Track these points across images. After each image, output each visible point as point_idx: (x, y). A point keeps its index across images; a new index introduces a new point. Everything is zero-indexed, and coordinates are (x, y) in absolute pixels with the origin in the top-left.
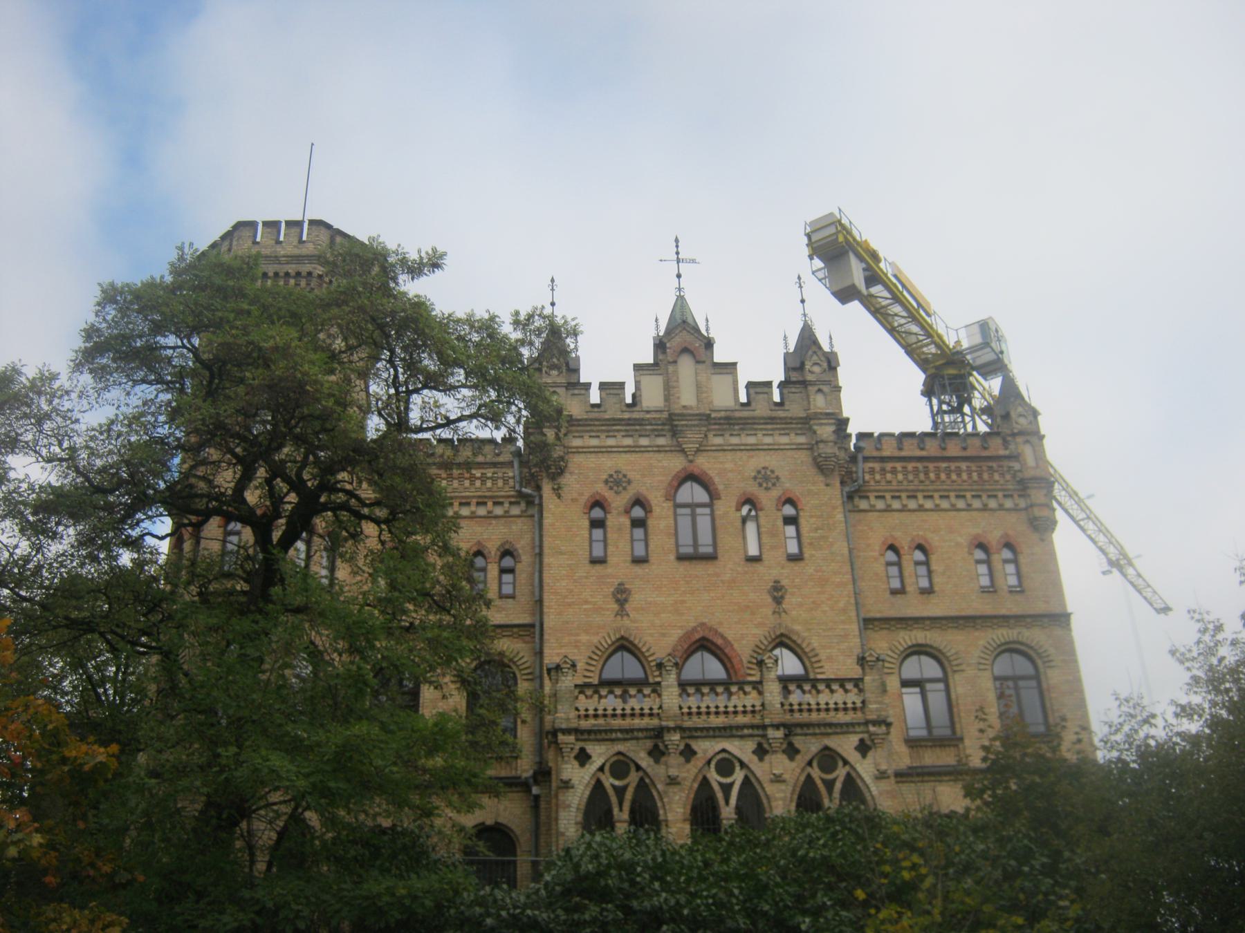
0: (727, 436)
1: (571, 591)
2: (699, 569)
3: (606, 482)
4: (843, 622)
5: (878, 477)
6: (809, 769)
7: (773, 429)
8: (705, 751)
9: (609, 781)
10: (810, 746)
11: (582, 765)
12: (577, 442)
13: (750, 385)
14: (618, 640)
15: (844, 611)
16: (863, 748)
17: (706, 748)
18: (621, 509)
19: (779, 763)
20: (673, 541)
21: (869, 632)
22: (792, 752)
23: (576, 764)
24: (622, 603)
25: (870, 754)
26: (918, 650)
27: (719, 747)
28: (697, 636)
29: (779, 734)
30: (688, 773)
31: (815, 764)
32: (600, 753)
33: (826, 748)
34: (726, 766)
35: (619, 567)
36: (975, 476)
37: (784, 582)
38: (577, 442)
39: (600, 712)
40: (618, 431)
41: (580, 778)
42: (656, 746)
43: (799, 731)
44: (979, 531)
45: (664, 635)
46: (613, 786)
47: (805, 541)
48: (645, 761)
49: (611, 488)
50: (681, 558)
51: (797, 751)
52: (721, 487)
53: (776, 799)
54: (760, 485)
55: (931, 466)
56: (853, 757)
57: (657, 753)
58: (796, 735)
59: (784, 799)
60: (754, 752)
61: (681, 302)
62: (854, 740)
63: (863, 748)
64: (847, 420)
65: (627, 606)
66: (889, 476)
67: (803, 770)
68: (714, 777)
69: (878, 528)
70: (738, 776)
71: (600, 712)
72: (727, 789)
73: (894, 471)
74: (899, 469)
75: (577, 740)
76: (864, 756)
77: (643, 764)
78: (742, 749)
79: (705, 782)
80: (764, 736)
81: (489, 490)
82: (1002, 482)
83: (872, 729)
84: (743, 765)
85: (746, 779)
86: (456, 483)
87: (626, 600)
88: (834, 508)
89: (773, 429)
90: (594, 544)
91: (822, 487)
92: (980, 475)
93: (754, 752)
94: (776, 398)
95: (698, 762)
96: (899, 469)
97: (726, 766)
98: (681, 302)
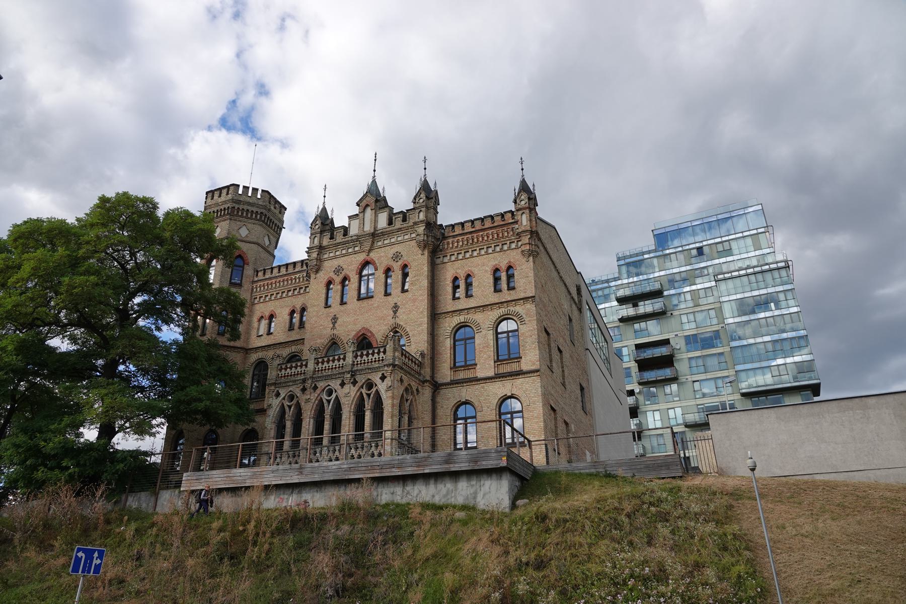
2: (365, 301)
9: (286, 403)
10: (361, 379)
15: (422, 312)
17: (321, 385)
22: (355, 383)
24: (334, 323)
25: (634, 348)
30: (314, 396)
35: (396, 296)
41: (275, 403)
55: (475, 235)
61: (374, 182)
63: (383, 378)
95: (318, 391)
97: (330, 393)
98: (374, 182)
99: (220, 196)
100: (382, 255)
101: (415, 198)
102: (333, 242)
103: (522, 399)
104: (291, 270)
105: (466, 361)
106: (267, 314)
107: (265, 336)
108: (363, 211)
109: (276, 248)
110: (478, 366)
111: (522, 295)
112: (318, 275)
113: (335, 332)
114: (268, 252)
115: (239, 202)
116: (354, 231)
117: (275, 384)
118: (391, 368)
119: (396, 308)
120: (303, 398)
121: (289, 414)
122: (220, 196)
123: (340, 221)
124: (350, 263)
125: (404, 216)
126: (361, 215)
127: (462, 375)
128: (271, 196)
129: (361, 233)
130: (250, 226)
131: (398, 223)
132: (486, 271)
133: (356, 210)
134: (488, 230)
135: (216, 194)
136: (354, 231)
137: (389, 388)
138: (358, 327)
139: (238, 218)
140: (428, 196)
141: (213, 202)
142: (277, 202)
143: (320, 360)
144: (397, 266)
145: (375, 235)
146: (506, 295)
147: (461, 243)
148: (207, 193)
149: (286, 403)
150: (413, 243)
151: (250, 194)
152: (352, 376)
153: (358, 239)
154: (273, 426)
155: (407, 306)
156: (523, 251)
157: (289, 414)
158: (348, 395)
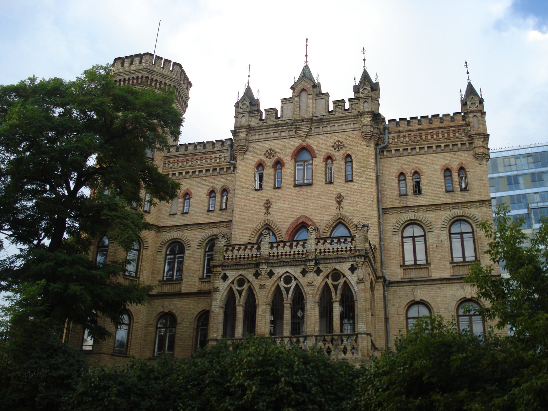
0: (321, 128)
1: (246, 205)
3: (265, 154)
4: (370, 211)
5: (396, 140)
6: (327, 280)
7: (342, 122)
8: (278, 273)
9: (235, 287)
10: (326, 269)
11: (224, 281)
12: (253, 138)
13: (334, 102)
14: (265, 225)
15: (370, 205)
16: (353, 269)
17: (279, 271)
18: (271, 166)
19: (311, 276)
20: (293, 178)
21: (386, 215)
22: (318, 272)
23: (221, 280)
24: (267, 208)
26: (412, 223)
27: (284, 271)
28: (300, 222)
29: (313, 263)
30: (270, 283)
31: (330, 277)
32: (232, 275)
33: (335, 269)
34: (288, 280)
36: (446, 135)
37: (343, 194)
38: (253, 138)
40: (271, 130)
41: (222, 286)
42: (257, 271)
43: (322, 262)
44: (447, 162)
45: (285, 222)
46: (237, 290)
47: (354, 174)
48: (251, 277)
49: (267, 157)
50: (295, 186)
51: (321, 271)
52: (316, 152)
53: (309, 294)
54: (335, 149)
56: (348, 273)
57: (257, 275)
58: (321, 264)
59: (312, 294)
60: (301, 273)
62: (349, 265)
63: (353, 269)
64: (489, 135)
65: (269, 210)
66: (402, 139)
67: (323, 280)
68: (282, 284)
69: (393, 166)
70: (293, 284)
71: (246, 256)
72: (287, 290)
73: (404, 137)
74: (407, 135)
75: (223, 270)
76: (353, 273)
77: (250, 280)
78: (295, 271)
79: (278, 287)
80: (306, 265)
81: (218, 163)
82: (460, 137)
83: (357, 259)
84: (296, 279)
85: (297, 285)
86: (204, 161)
87: (269, 207)
88: (370, 157)
89: (342, 122)
91: (365, 147)
92: (448, 135)
93: (301, 273)
94: (347, 106)
95: (274, 278)
96: (407, 135)
97: (288, 280)
98: (306, 67)
99: (131, 64)
105: (464, 257)
107: (179, 215)
110: (432, 266)
111: (477, 198)
112: (246, 156)
113: (269, 217)
115: (151, 72)
117: (222, 266)
118: (363, 259)
119: (339, 199)
120: (256, 283)
121: (241, 301)
122: (131, 64)
124: (286, 147)
126: (297, 99)
127: (413, 274)
128: (183, 72)
129: (297, 117)
133: (289, 94)
134: (425, 132)
135: (137, 60)
137: (360, 281)
138: (297, 215)
140: (367, 88)
141: (123, 70)
142: (186, 78)
144: (339, 155)
146: (459, 197)
148: (116, 60)
149: (235, 287)
150: (356, 133)
152: (316, 264)
154: (221, 311)
155: (353, 197)
157: (241, 301)
158: (313, 284)
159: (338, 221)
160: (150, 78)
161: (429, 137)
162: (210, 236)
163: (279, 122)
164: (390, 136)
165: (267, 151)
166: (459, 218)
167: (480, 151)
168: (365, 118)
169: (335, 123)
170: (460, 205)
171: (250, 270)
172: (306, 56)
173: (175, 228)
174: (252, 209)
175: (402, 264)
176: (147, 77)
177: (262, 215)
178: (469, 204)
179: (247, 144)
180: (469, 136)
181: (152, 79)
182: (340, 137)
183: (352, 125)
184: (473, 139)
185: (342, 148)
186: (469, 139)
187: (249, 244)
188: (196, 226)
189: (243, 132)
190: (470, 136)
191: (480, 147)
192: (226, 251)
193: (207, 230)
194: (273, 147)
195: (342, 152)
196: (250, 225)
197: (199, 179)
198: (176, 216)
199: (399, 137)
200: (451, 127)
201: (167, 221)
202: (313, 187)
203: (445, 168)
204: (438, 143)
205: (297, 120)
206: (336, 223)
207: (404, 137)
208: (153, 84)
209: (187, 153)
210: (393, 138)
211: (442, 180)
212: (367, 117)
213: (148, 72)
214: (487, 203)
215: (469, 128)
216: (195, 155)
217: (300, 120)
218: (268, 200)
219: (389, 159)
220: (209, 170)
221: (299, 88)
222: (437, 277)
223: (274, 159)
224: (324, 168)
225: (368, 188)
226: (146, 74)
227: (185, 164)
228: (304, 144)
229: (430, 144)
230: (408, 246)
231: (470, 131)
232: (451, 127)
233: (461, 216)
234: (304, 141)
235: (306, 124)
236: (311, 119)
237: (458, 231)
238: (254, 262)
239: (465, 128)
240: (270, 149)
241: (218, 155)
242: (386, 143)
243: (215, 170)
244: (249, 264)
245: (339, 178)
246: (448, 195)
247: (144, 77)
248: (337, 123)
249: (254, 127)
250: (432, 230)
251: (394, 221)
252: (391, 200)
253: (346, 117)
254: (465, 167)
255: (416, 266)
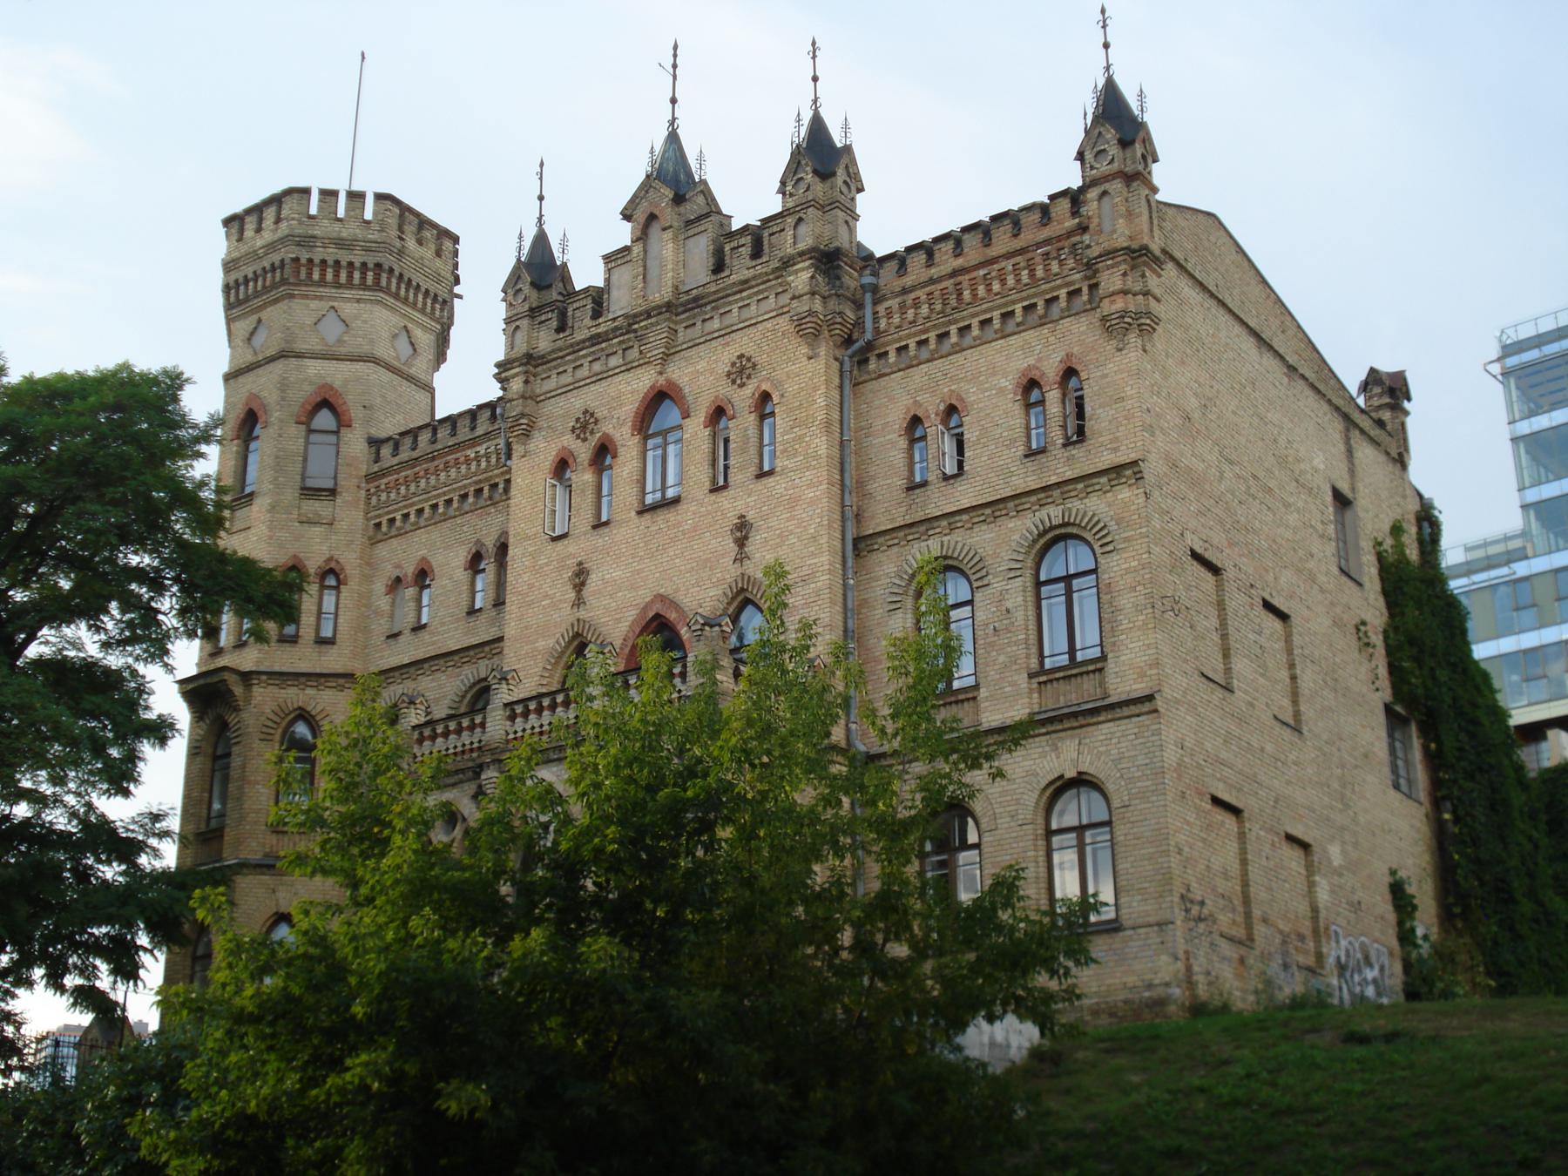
0: (699, 323)
2: (662, 517)
7: (749, 297)
21: (874, 556)
37: (750, 516)
39: (546, 728)
40: (584, 356)
44: (1032, 361)
45: (618, 621)
54: (734, 382)
61: (673, 138)
71: (460, 749)
81: (485, 471)
88: (815, 389)
89: (749, 297)
90: (332, 610)
92: (1032, 274)
98: (673, 138)
99: (259, 230)
100: (701, 373)
101: (783, 183)
102: (563, 340)
103: (1110, 787)
104: (464, 433)
105: (1072, 651)
106: (410, 570)
108: (642, 237)
109: (440, 357)
112: (532, 446)
113: (583, 614)
114: (410, 379)
115: (306, 241)
116: (621, 303)
119: (742, 531)
122: (259, 230)
123: (586, 273)
125: (757, 237)
128: (404, 209)
130: (348, 309)
131: (741, 267)
132: (1001, 391)
133: (623, 234)
136: (621, 303)
138: (644, 595)
139: (312, 290)
140: (821, 161)
142: (424, 223)
143: (519, 709)
145: (685, 307)
146: (1060, 466)
147: (925, 310)
150: (783, 322)
151: (341, 213)
153: (631, 325)
155: (774, 522)
156: (1104, 319)
159: (740, 598)
160: (303, 261)
161: (981, 290)
162: (474, 684)
163: (601, 330)
164: (881, 309)
165: (578, 420)
166: (1057, 532)
167: (1114, 308)
168: (797, 272)
169: (730, 303)
170: (1056, 493)
171: (466, 786)
172: (674, 101)
173: (397, 674)
174: (546, 596)
175: (1034, 663)
176: (296, 260)
177: (567, 606)
178: (1080, 486)
179: (527, 411)
180: (1087, 264)
181: (310, 261)
182: (743, 343)
183: (772, 299)
184: (1097, 271)
185: (749, 377)
186: (1089, 273)
187: (541, 696)
188: (442, 662)
189: (516, 375)
190: (1089, 265)
191: (1113, 294)
192: (420, 741)
193: (466, 667)
194: (592, 405)
195: (748, 390)
196: (541, 644)
197: (448, 524)
198: (402, 639)
199: (903, 309)
200: (1038, 245)
201: (382, 658)
202: (682, 507)
203: (1025, 381)
204: (1006, 305)
205: (635, 316)
206: (735, 604)
207: (916, 305)
208: (329, 276)
209: (415, 454)
210: (889, 315)
211: (1018, 420)
212: (803, 269)
213: (299, 244)
214: (1129, 472)
215: (1086, 238)
216: (433, 459)
217: (641, 314)
218: (580, 563)
219: (883, 382)
220: (947, 334)
221: (641, 216)
222: (995, 724)
223: (593, 441)
224: (706, 447)
225: (809, 486)
226: (289, 253)
227: (413, 488)
228: (661, 381)
229: (985, 311)
230: (1054, 608)
231: (1089, 246)
232: (1038, 245)
233: (1060, 526)
234: (661, 373)
235: (658, 323)
236: (669, 306)
237: (1059, 572)
238: (470, 764)
239: (1078, 238)
240: (741, 356)
241: (482, 449)
242: (869, 336)
243: (479, 492)
244: (462, 771)
245: (741, 469)
246: (1031, 466)
247: (287, 261)
248: (736, 301)
249: (543, 357)
250: (985, 582)
251: (892, 569)
252: (886, 510)
253: (754, 277)
254: (1079, 368)
255: (1075, 668)
